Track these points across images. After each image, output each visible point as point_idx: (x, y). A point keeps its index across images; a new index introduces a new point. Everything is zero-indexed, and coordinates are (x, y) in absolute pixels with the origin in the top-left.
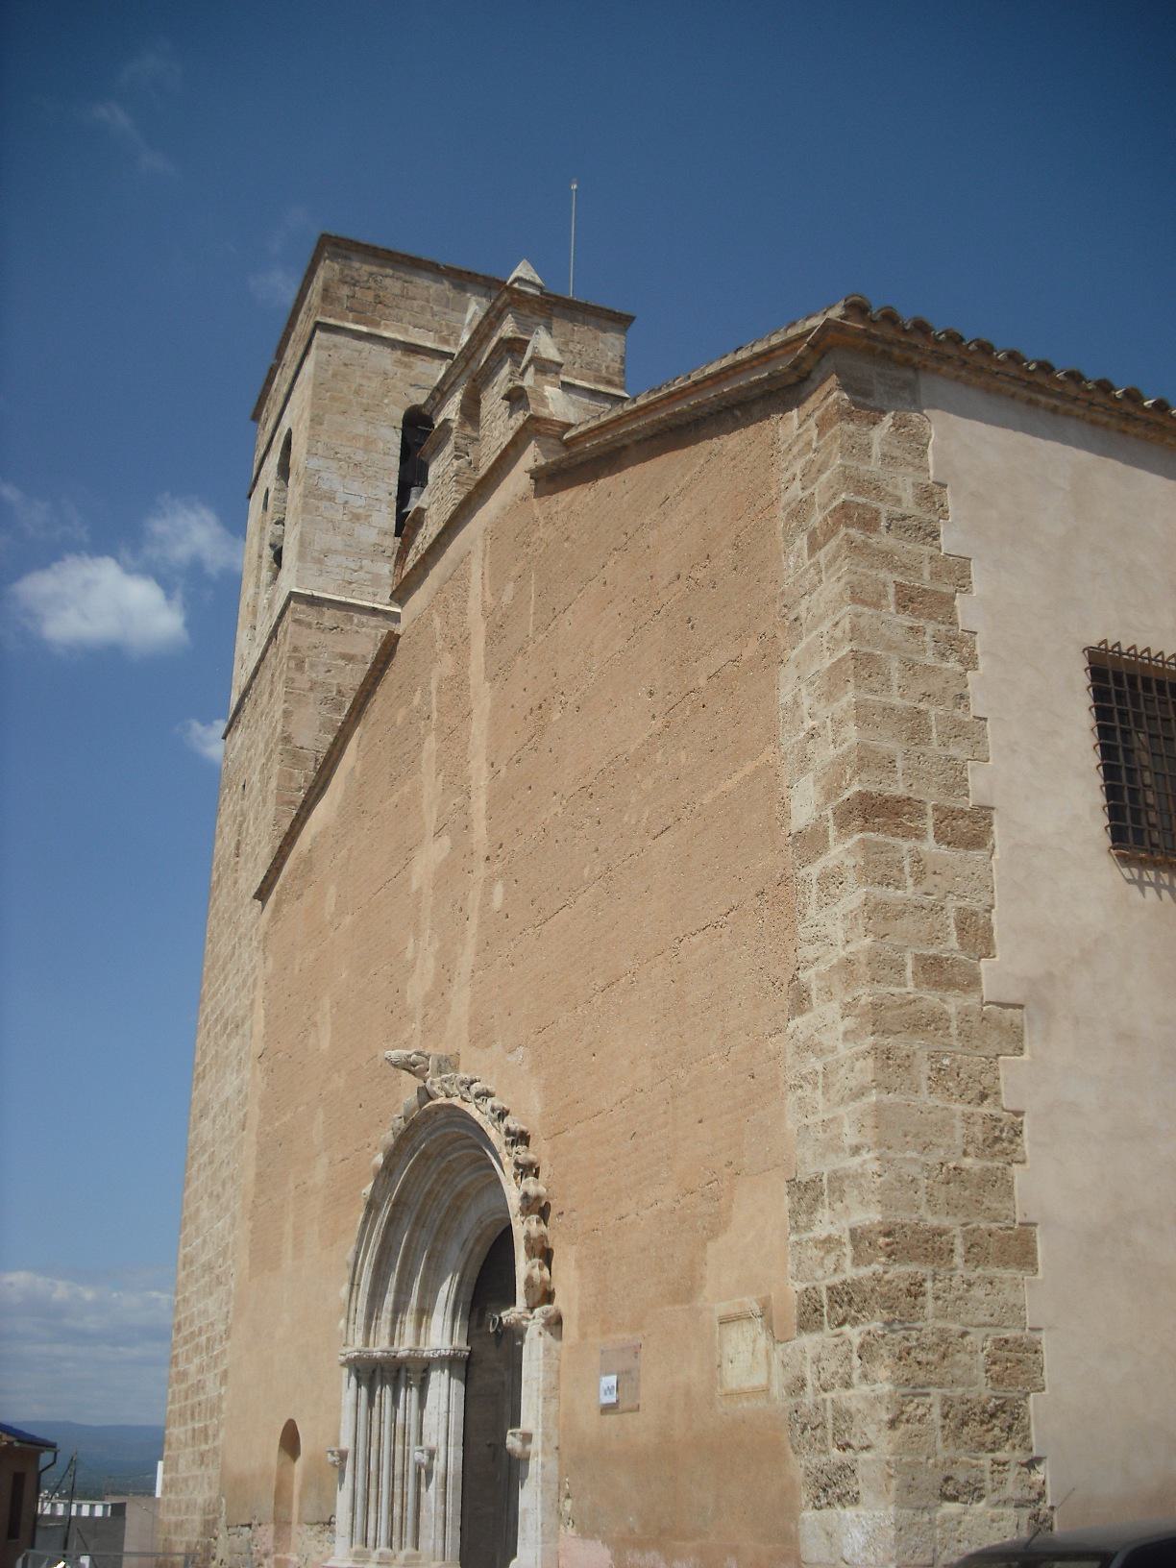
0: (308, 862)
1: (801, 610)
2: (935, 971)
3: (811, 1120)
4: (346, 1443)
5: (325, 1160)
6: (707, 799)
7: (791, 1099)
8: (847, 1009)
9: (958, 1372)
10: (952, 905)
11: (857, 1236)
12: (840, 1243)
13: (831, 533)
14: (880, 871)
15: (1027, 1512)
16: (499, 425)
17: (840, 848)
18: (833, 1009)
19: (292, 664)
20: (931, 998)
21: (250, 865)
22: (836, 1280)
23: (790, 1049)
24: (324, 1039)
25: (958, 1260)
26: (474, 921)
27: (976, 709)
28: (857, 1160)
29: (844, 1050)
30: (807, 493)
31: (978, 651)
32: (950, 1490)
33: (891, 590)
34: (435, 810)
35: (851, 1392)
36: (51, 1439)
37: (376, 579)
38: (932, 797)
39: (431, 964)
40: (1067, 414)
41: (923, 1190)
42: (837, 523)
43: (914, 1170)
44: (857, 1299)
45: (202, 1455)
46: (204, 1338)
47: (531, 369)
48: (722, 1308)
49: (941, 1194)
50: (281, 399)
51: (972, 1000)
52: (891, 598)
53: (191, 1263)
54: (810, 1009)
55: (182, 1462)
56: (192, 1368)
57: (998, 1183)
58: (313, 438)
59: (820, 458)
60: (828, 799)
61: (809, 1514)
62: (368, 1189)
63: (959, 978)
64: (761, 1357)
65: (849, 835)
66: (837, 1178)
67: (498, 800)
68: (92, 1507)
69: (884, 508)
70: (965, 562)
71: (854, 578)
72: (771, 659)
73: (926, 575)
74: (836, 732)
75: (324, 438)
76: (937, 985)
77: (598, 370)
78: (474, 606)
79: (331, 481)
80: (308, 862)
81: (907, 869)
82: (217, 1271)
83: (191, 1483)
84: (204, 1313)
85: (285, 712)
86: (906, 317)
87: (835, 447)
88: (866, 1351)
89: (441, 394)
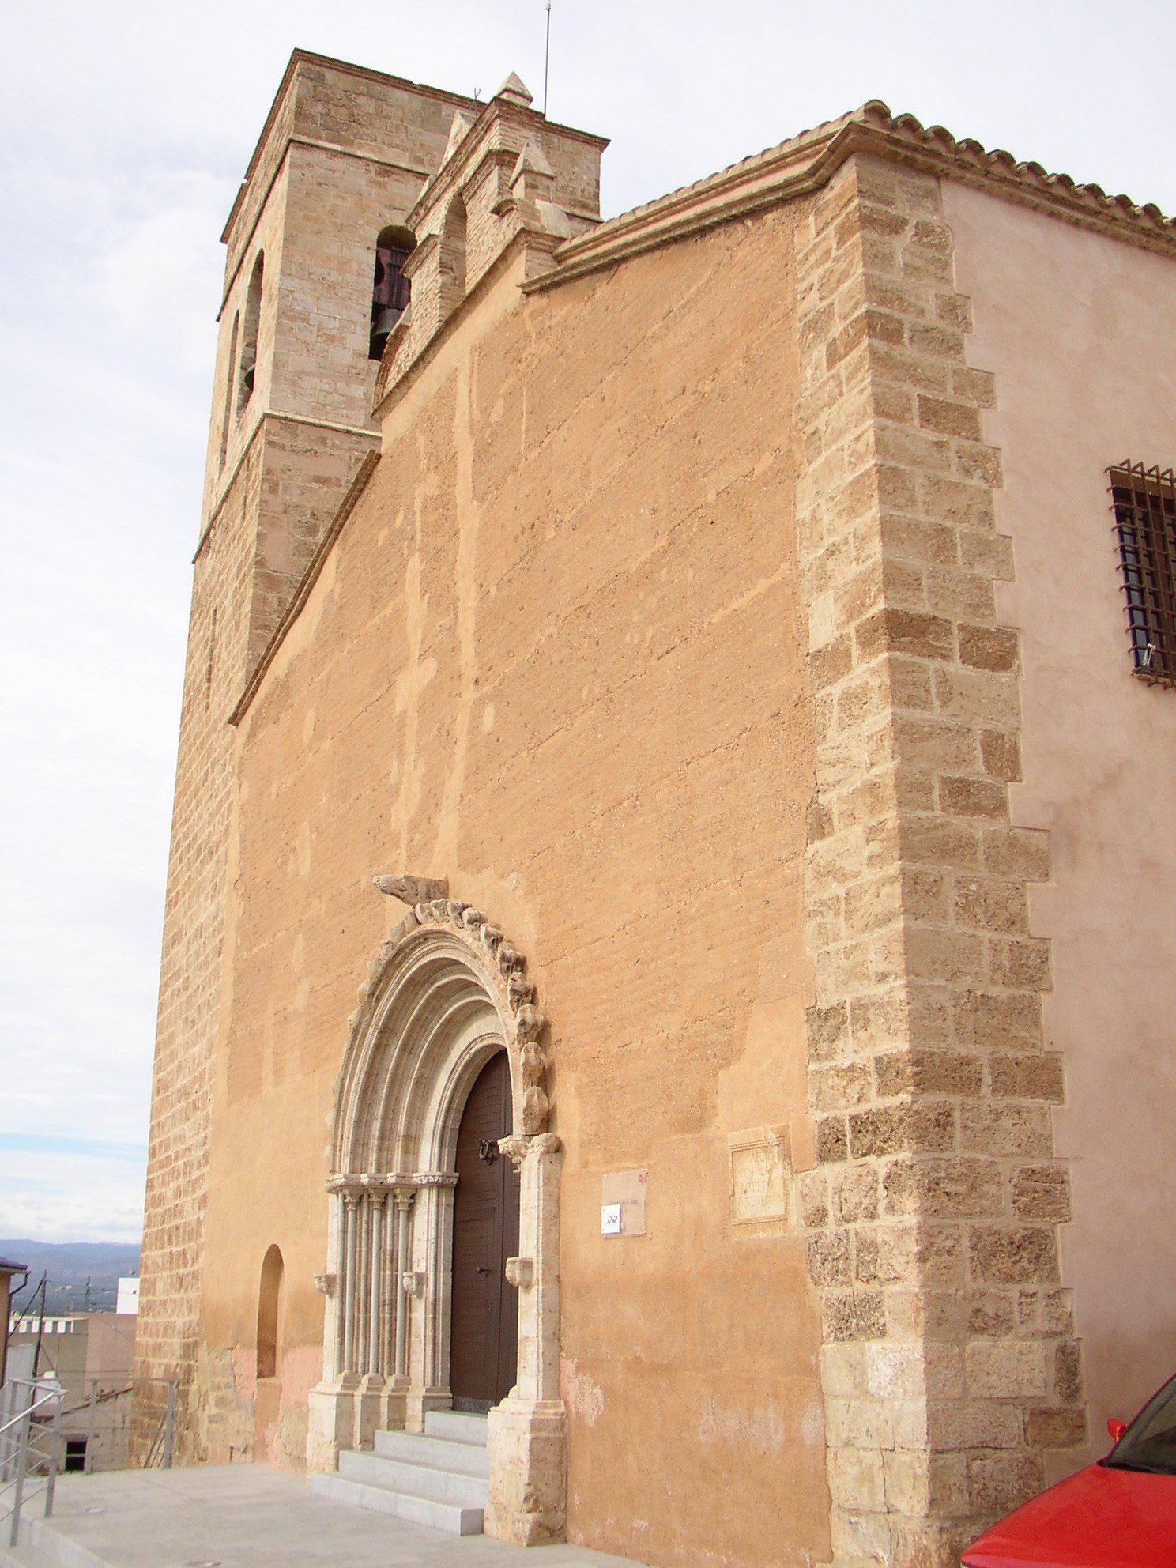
0: (284, 687)
1: (819, 423)
2: (961, 794)
3: (832, 947)
4: (333, 1269)
5: (305, 986)
6: (716, 618)
7: (811, 925)
8: (872, 833)
9: (986, 1203)
10: (978, 726)
11: (883, 1065)
12: (864, 1070)
13: (851, 345)
14: (904, 689)
15: (1055, 1343)
16: (487, 236)
17: (864, 666)
18: (857, 833)
19: (266, 486)
20: (959, 823)
21: (223, 690)
22: (861, 1109)
23: (809, 875)
24: (303, 864)
25: (985, 1090)
26: (461, 749)
27: (1001, 528)
28: (882, 989)
29: (869, 875)
30: (825, 303)
31: (1003, 468)
32: (979, 1324)
33: (915, 403)
34: (420, 631)
35: (877, 1222)
36: (21, 1263)
37: (350, 403)
38: (957, 616)
39: (417, 788)
40: (1090, 228)
41: (950, 1019)
42: (859, 334)
43: (943, 999)
44: (884, 1129)
45: (181, 1279)
46: (181, 1162)
47: (522, 181)
48: (734, 1138)
49: (968, 1022)
50: (252, 220)
51: (999, 825)
52: (915, 411)
53: (166, 1089)
54: (831, 833)
55: (159, 1286)
56: (170, 1193)
57: (1026, 1012)
58: (287, 258)
59: (841, 267)
60: (851, 617)
61: (830, 1347)
62: (353, 1016)
63: (985, 803)
64: (778, 1189)
65: (875, 654)
66: (860, 1006)
67: (488, 620)
68: (55, 1323)
69: (908, 319)
70: (988, 377)
71: (879, 390)
72: (787, 473)
73: (950, 389)
74: (859, 548)
75: (298, 258)
76: (964, 809)
77: (572, 193)
78: (461, 423)
79: (305, 300)
80: (284, 687)
81: (933, 690)
82: (193, 1097)
83: (170, 1306)
84: (181, 1138)
85: (259, 534)
86: (926, 123)
87: (858, 255)
88: (892, 1181)
89: (423, 207)
